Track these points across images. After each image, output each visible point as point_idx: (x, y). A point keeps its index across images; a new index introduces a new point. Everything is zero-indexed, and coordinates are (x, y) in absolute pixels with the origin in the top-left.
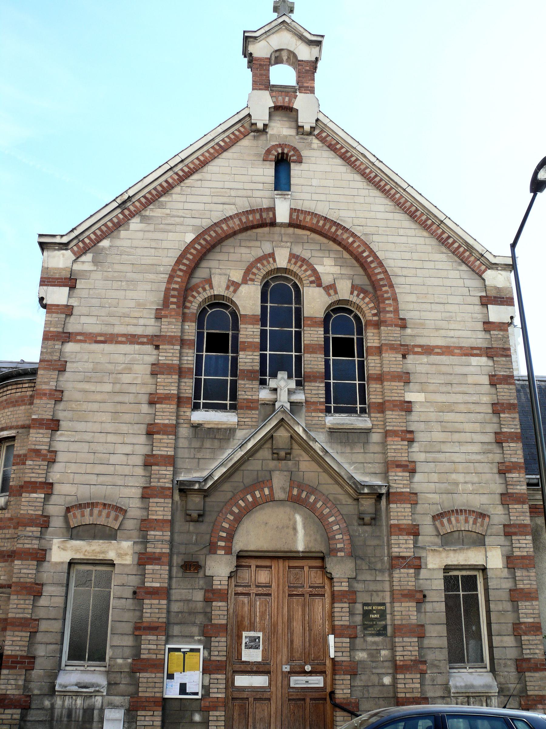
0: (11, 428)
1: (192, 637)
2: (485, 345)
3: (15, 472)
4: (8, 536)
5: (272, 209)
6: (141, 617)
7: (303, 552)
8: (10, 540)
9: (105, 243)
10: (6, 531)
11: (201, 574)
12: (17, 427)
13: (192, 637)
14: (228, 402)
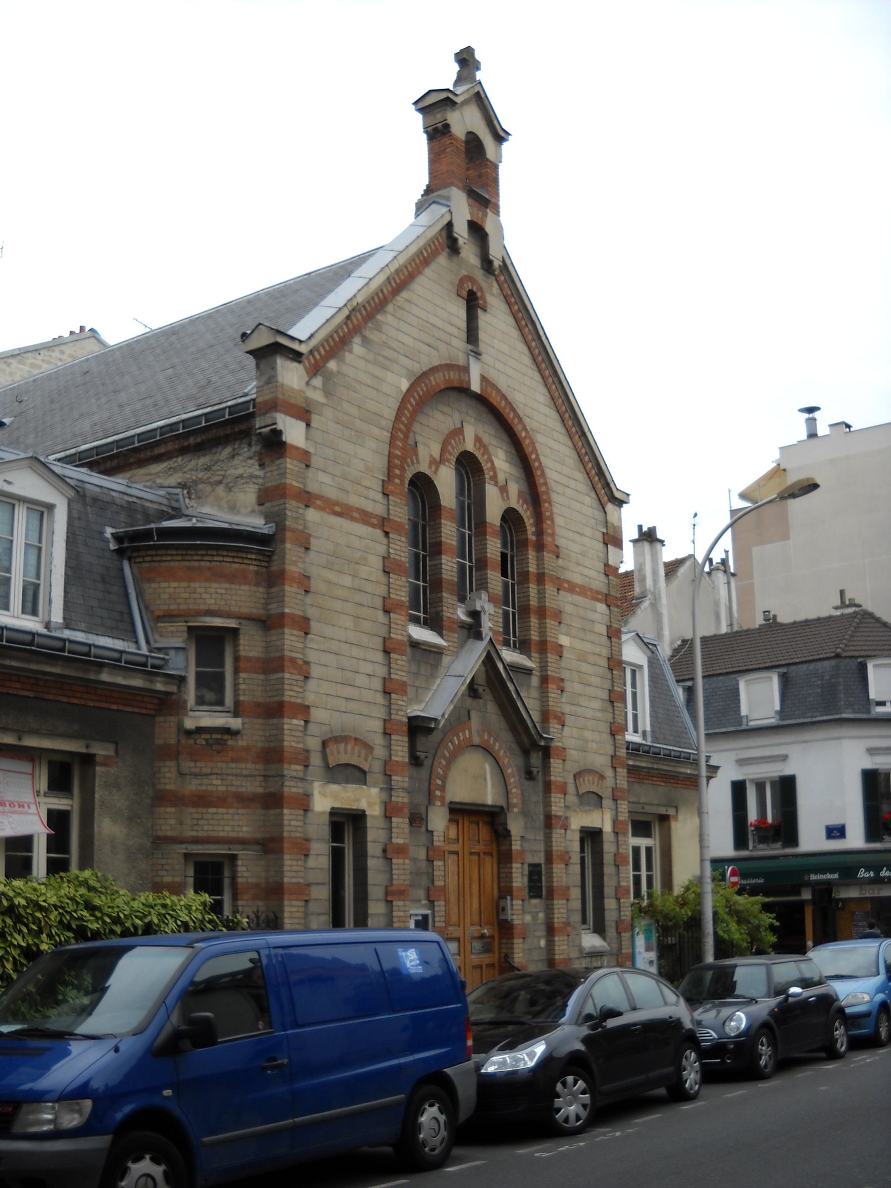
0: (228, 615)
1: (419, 901)
2: (604, 590)
3: (246, 681)
4: (245, 772)
5: (466, 369)
6: (391, 879)
7: (492, 806)
8: (249, 779)
9: (332, 365)
10: (242, 765)
11: (423, 829)
12: (238, 617)
13: (419, 901)
14: (422, 615)
